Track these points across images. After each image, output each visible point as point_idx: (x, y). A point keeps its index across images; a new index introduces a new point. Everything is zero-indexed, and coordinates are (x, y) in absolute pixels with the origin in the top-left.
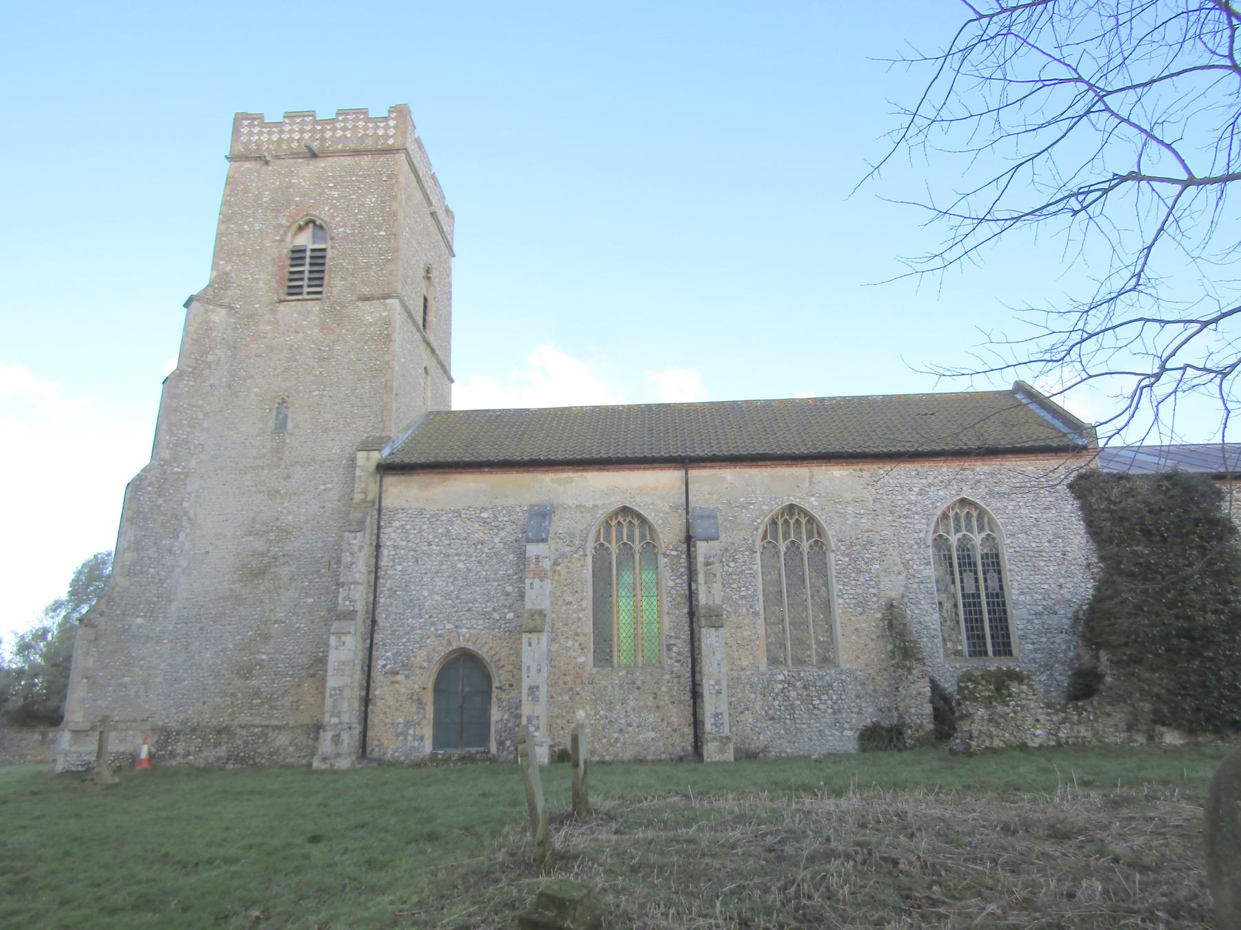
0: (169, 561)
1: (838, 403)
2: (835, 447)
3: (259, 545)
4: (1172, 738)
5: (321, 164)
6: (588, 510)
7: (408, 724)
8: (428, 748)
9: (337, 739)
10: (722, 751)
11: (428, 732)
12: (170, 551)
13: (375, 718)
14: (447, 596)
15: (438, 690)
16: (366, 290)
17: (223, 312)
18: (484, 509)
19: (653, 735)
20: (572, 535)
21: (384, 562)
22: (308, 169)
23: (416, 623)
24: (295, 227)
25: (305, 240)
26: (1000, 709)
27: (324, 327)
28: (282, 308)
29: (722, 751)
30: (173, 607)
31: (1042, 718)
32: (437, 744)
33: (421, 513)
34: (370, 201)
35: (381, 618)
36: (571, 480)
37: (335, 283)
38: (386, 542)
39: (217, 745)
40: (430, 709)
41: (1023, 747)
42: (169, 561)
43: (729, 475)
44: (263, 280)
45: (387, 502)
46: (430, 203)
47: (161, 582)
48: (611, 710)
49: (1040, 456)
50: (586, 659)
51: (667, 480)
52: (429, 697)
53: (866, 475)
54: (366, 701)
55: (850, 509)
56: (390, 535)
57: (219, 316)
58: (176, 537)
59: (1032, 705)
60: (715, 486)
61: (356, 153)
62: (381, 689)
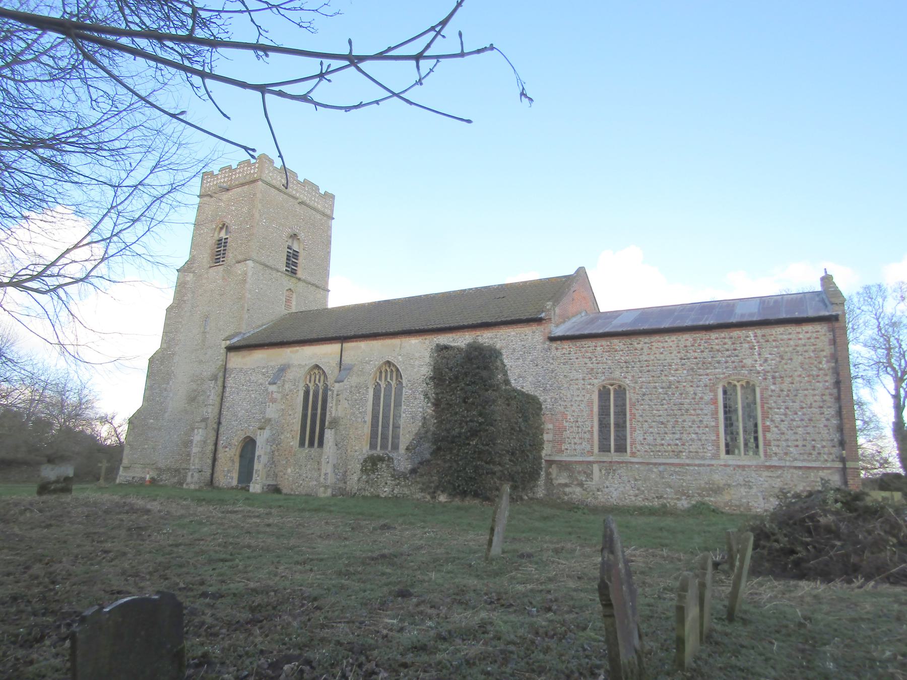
0: (165, 394)
1: (495, 289)
2: (407, 327)
3: (194, 386)
4: (443, 498)
5: (230, 193)
6: (303, 366)
7: (229, 471)
8: (235, 483)
9: (192, 476)
10: (325, 493)
11: (235, 475)
12: (166, 390)
13: (217, 468)
14: (247, 411)
15: (241, 456)
16: (240, 257)
17: (191, 275)
18: (264, 368)
19: (315, 483)
20: (295, 380)
21: (227, 394)
22: (225, 196)
23: (234, 423)
24: (218, 229)
25: (223, 235)
26: (372, 476)
27: (224, 278)
28: (211, 270)
29: (325, 493)
30: (166, 415)
31: (389, 482)
32: (239, 481)
33: (241, 370)
34: (245, 210)
35: (223, 421)
36: (297, 351)
37: (230, 256)
38: (228, 385)
39: (175, 476)
40: (237, 465)
41: (378, 496)
42: (165, 394)
43: (363, 345)
44: (205, 258)
45: (230, 365)
46: (296, 198)
47: (162, 403)
48: (300, 469)
49: (519, 326)
50: (295, 443)
51: (333, 349)
52: (237, 459)
53: (427, 342)
54: (214, 460)
55: (417, 363)
56: (230, 382)
57: (190, 277)
58: (168, 384)
59: (385, 474)
60: (357, 351)
61: (243, 185)
62: (220, 455)
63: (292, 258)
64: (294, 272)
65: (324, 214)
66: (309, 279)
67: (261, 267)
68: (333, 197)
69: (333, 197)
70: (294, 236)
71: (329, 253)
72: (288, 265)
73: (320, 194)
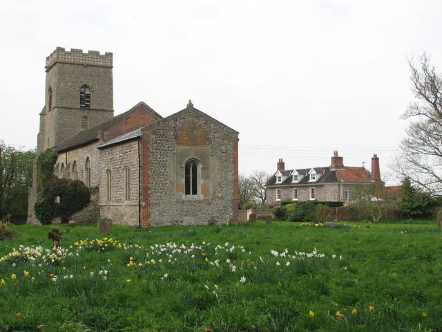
44: (48, 107)
63: (85, 101)
64: (88, 106)
65: (103, 67)
66: (98, 107)
67: (62, 110)
68: (111, 54)
69: (111, 54)
70: (85, 86)
71: (112, 89)
72: (81, 103)
73: (102, 57)
